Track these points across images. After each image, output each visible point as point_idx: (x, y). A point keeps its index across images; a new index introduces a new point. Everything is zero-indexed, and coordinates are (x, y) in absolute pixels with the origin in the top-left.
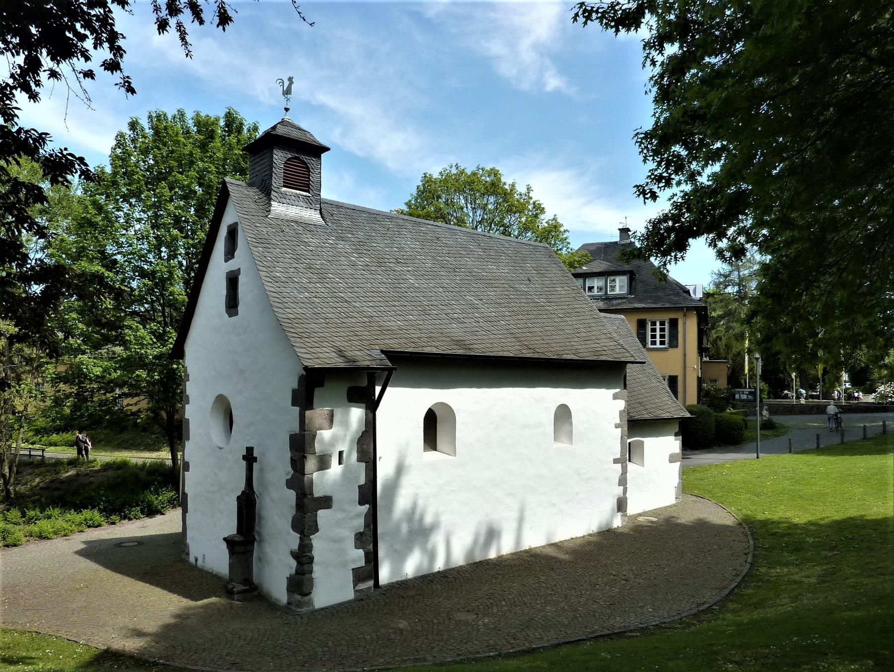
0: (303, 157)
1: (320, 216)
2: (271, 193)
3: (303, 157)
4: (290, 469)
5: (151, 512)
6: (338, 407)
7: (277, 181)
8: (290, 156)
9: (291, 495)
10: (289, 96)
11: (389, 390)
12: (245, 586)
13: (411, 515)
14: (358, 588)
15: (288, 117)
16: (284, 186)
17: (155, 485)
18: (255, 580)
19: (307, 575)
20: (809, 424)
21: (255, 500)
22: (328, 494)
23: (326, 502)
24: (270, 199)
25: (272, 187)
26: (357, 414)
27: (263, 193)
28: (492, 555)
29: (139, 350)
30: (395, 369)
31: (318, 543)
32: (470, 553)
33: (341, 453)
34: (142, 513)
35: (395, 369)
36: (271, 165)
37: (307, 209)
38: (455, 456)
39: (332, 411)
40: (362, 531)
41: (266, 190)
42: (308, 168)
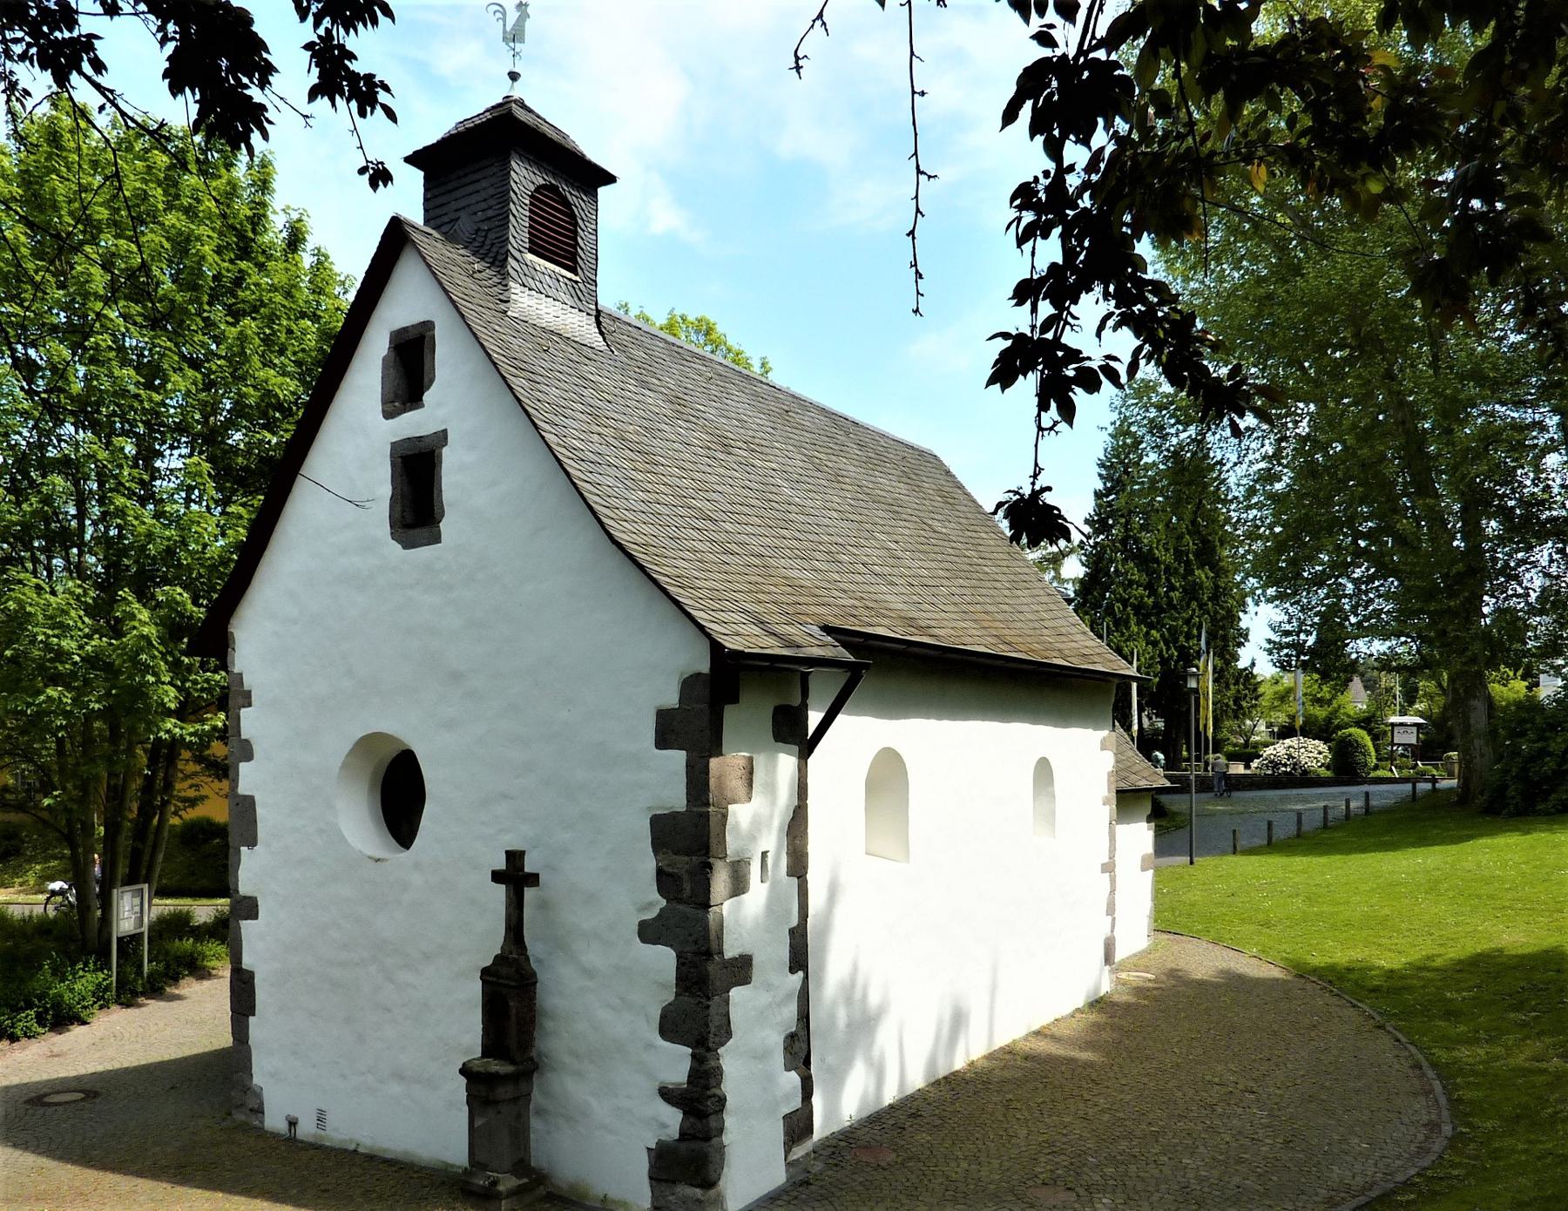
0: (565, 189)
1: (597, 330)
2: (506, 259)
3: (565, 189)
4: (655, 896)
5: (62, 1018)
6: (759, 752)
7: (518, 232)
8: (542, 182)
9: (664, 959)
10: (518, 46)
11: (841, 719)
12: (519, 1177)
13: (849, 991)
14: (793, 1156)
15: (518, 91)
16: (531, 251)
17: (51, 957)
18: (538, 1159)
19: (715, 1140)
20: (1211, 807)
21: (534, 974)
22: (747, 951)
23: (742, 969)
24: (504, 276)
25: (510, 247)
26: (787, 762)
27: (482, 259)
28: (959, 1064)
29: (55, 640)
30: (867, 667)
31: (732, 1062)
32: (932, 1063)
33: (764, 854)
34: (41, 1021)
35: (867, 667)
36: (503, 196)
37: (573, 310)
38: (908, 862)
39: (751, 760)
40: (794, 1029)
41: (495, 255)
42: (573, 216)
